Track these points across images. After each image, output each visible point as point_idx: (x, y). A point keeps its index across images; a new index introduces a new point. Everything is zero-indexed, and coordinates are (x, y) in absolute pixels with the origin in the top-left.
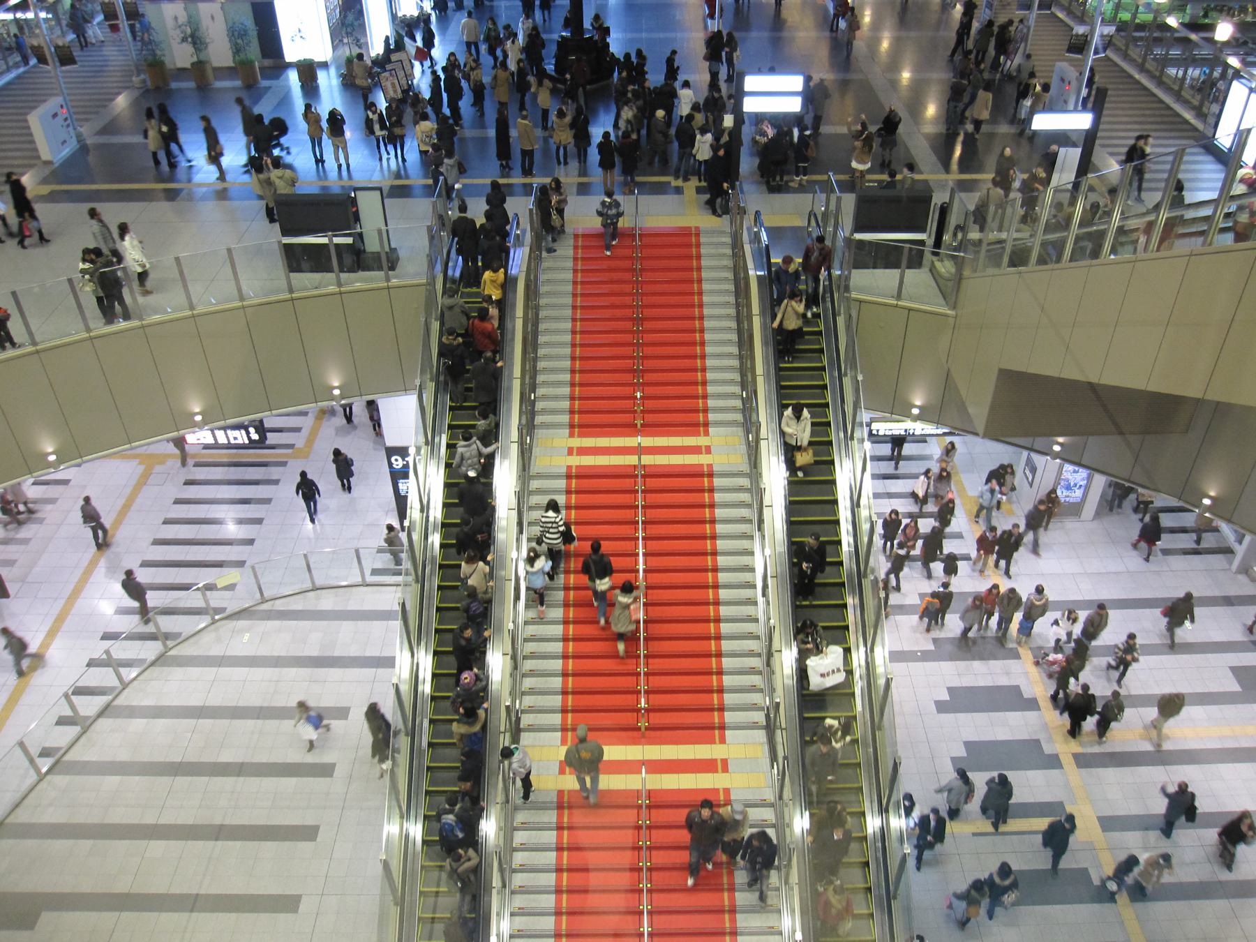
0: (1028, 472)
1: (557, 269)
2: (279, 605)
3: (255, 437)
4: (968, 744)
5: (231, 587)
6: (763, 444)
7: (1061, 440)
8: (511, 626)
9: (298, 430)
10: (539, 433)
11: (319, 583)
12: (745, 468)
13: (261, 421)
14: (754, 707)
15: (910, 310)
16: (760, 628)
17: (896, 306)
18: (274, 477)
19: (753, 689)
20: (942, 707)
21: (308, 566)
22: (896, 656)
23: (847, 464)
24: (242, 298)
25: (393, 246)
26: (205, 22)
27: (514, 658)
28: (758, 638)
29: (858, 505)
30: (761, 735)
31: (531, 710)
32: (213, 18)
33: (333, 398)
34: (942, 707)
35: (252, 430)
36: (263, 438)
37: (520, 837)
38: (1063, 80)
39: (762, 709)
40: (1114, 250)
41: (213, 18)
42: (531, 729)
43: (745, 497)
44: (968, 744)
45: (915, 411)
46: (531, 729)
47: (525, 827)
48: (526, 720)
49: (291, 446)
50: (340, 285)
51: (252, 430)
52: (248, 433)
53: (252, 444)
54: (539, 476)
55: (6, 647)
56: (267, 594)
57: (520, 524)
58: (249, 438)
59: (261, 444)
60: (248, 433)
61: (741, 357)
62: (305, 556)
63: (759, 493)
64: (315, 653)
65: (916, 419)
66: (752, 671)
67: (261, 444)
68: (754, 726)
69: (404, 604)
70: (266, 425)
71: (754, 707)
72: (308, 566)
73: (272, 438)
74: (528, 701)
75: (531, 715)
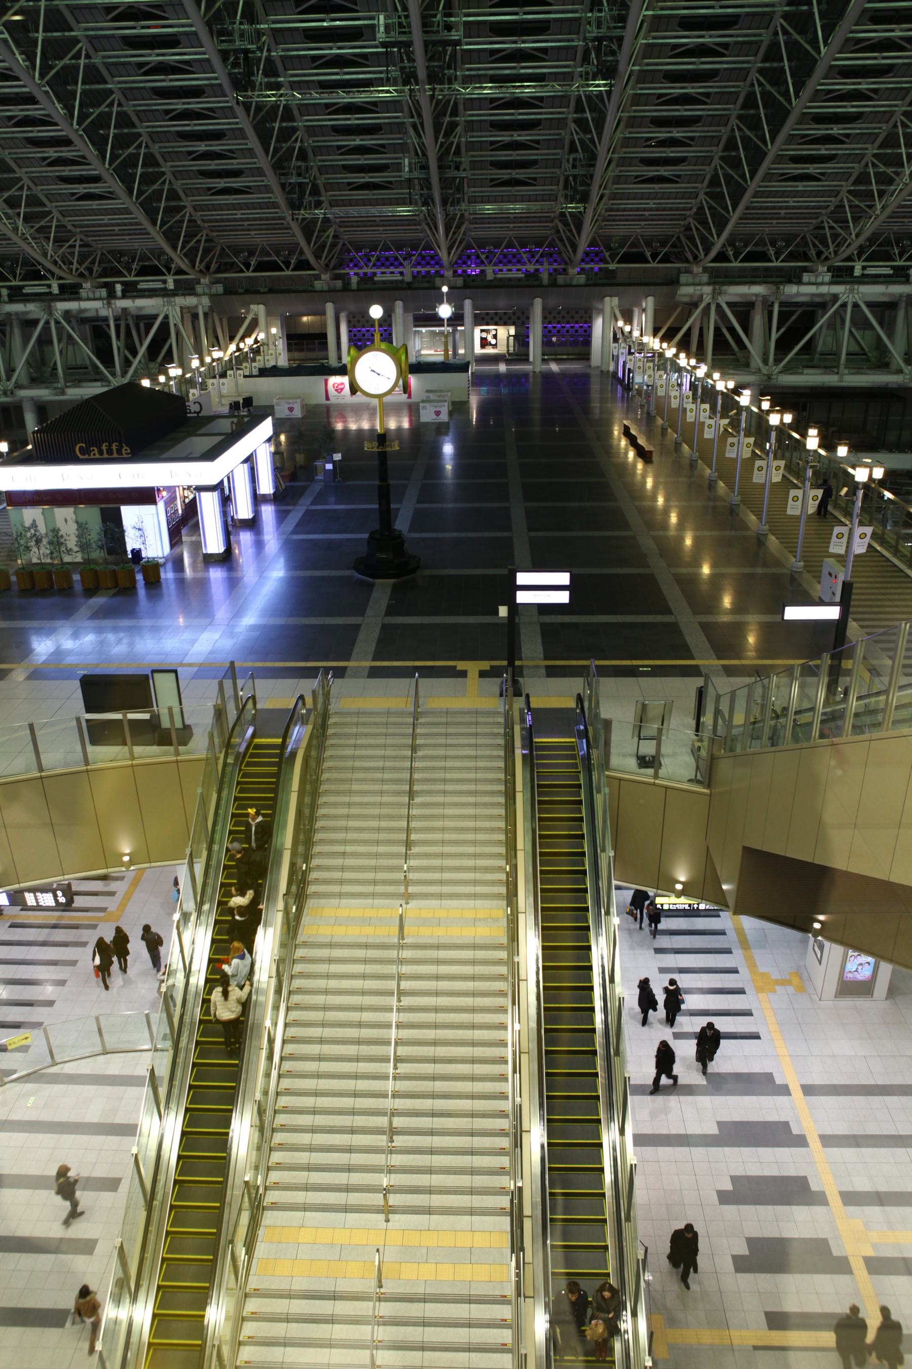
0: (816, 949)
1: (341, 746)
2: (69, 1069)
3: (62, 900)
4: (751, 1241)
5: (24, 1049)
6: (521, 917)
7: (821, 917)
8: (258, 1096)
9: (112, 894)
10: (311, 903)
11: (109, 1047)
12: (505, 941)
13: (69, 885)
14: (502, 1191)
15: (666, 788)
16: (507, 1106)
17: (654, 784)
18: (83, 940)
19: (501, 1171)
20: (724, 1198)
21: (100, 1030)
22: (640, 1140)
23: (602, 940)
24: (41, 769)
25: (187, 722)
26: (60, 524)
27: (261, 1129)
28: (507, 1116)
29: (612, 980)
30: (505, 1222)
31: (277, 1186)
32: (66, 521)
33: (122, 864)
34: (724, 1198)
35: (59, 893)
36: (70, 901)
37: (249, 1329)
38: (830, 574)
39: (506, 1194)
40: (822, 736)
41: (66, 521)
42: (275, 1207)
43: (503, 970)
44: (751, 1241)
45: (679, 887)
46: (275, 1207)
47: (256, 1317)
48: (272, 1197)
49: (103, 910)
50: (177, 754)
51: (59, 893)
52: (55, 896)
53: (59, 907)
54: (305, 944)
55: (786, 1124)
56: (58, 1059)
57: (278, 991)
58: (56, 901)
59: (68, 906)
60: (55, 896)
61: (506, 832)
62: (97, 1019)
63: (514, 968)
64: (95, 1120)
65: (679, 894)
66: (501, 1152)
67: (68, 906)
68: (500, 1212)
69: (152, 1071)
70: (74, 888)
71: (502, 1191)
72: (100, 1030)
73: (79, 901)
74: (274, 1176)
75: (276, 1192)
